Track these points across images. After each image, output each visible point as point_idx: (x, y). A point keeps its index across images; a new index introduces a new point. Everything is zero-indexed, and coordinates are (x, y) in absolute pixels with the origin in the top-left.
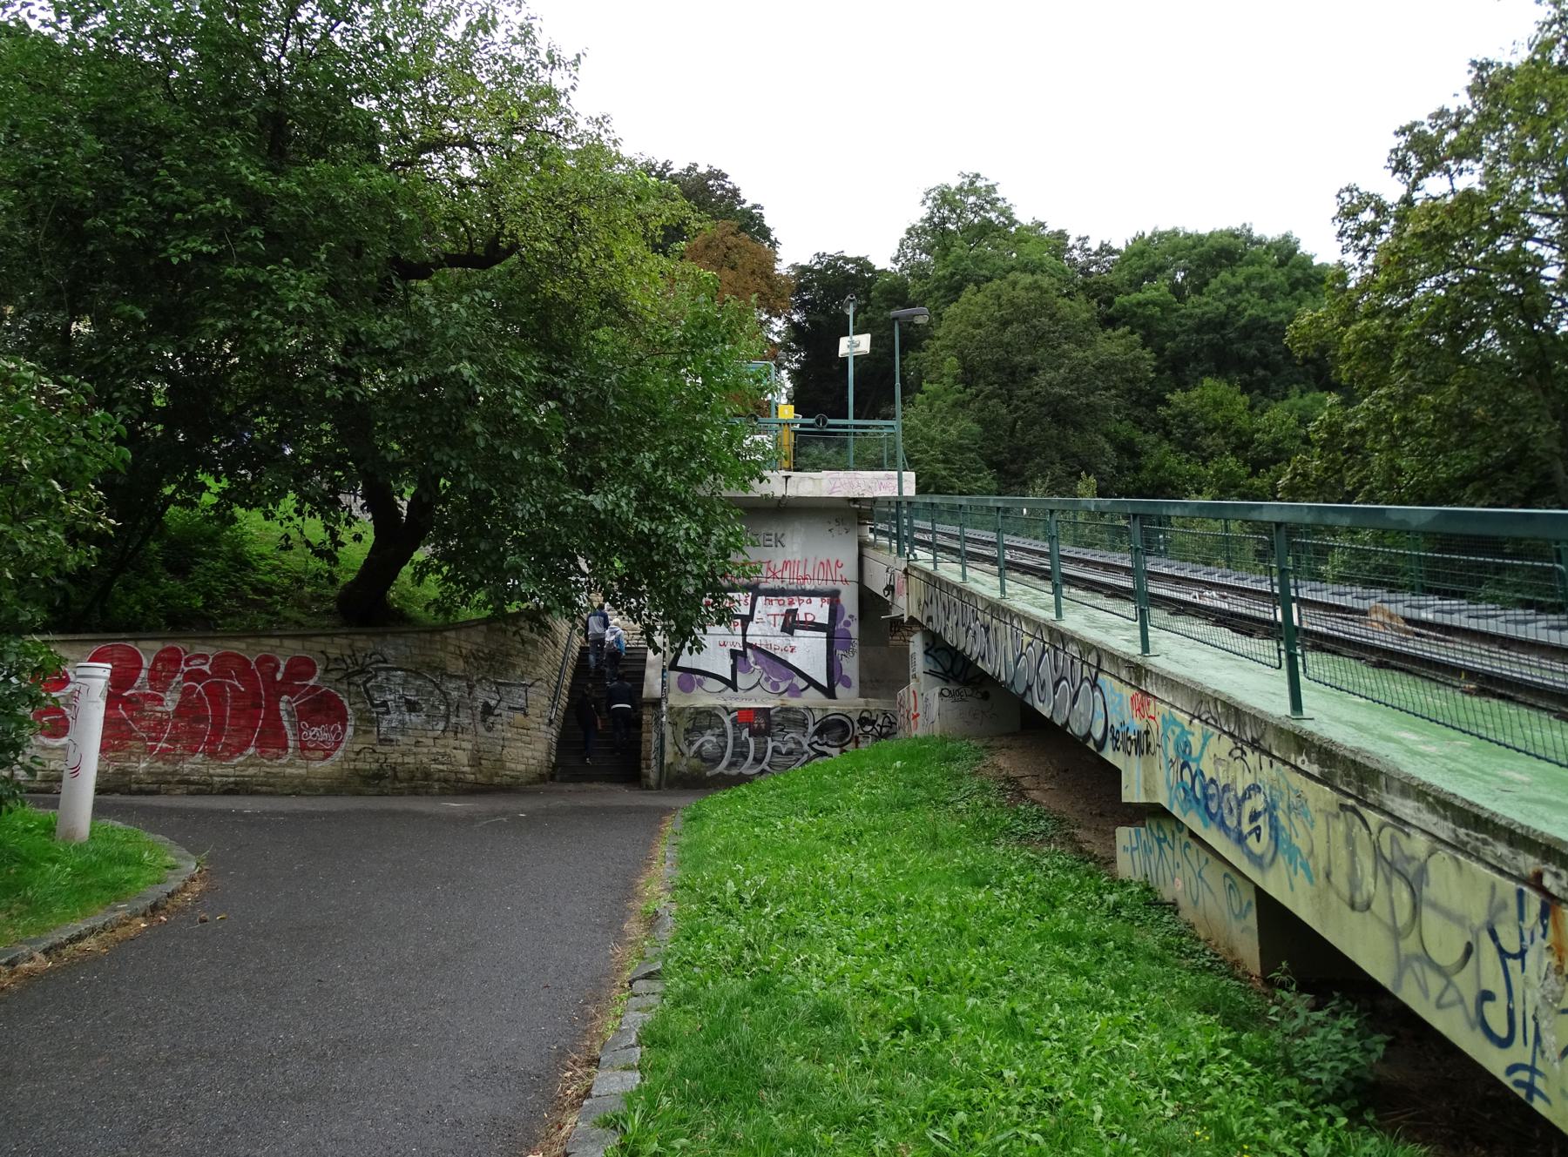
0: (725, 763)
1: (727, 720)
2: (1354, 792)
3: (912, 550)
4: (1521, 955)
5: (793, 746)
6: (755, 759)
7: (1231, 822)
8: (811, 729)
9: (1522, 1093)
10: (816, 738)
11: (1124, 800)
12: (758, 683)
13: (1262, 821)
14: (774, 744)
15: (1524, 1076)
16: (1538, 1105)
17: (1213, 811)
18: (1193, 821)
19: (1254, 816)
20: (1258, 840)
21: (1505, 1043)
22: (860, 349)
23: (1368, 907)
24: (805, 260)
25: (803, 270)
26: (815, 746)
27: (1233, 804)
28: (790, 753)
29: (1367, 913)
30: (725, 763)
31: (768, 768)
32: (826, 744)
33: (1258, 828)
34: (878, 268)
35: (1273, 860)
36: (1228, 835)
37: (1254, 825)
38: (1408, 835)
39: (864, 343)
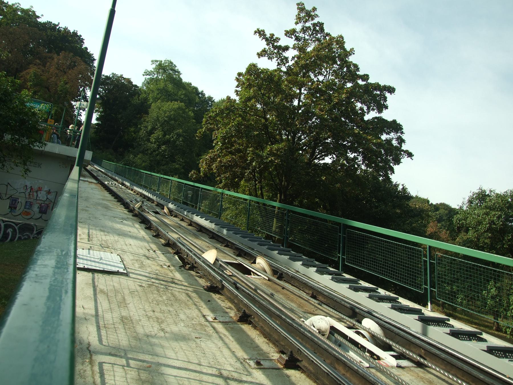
10: (36, 236)
12: (20, 214)
14: (20, 235)
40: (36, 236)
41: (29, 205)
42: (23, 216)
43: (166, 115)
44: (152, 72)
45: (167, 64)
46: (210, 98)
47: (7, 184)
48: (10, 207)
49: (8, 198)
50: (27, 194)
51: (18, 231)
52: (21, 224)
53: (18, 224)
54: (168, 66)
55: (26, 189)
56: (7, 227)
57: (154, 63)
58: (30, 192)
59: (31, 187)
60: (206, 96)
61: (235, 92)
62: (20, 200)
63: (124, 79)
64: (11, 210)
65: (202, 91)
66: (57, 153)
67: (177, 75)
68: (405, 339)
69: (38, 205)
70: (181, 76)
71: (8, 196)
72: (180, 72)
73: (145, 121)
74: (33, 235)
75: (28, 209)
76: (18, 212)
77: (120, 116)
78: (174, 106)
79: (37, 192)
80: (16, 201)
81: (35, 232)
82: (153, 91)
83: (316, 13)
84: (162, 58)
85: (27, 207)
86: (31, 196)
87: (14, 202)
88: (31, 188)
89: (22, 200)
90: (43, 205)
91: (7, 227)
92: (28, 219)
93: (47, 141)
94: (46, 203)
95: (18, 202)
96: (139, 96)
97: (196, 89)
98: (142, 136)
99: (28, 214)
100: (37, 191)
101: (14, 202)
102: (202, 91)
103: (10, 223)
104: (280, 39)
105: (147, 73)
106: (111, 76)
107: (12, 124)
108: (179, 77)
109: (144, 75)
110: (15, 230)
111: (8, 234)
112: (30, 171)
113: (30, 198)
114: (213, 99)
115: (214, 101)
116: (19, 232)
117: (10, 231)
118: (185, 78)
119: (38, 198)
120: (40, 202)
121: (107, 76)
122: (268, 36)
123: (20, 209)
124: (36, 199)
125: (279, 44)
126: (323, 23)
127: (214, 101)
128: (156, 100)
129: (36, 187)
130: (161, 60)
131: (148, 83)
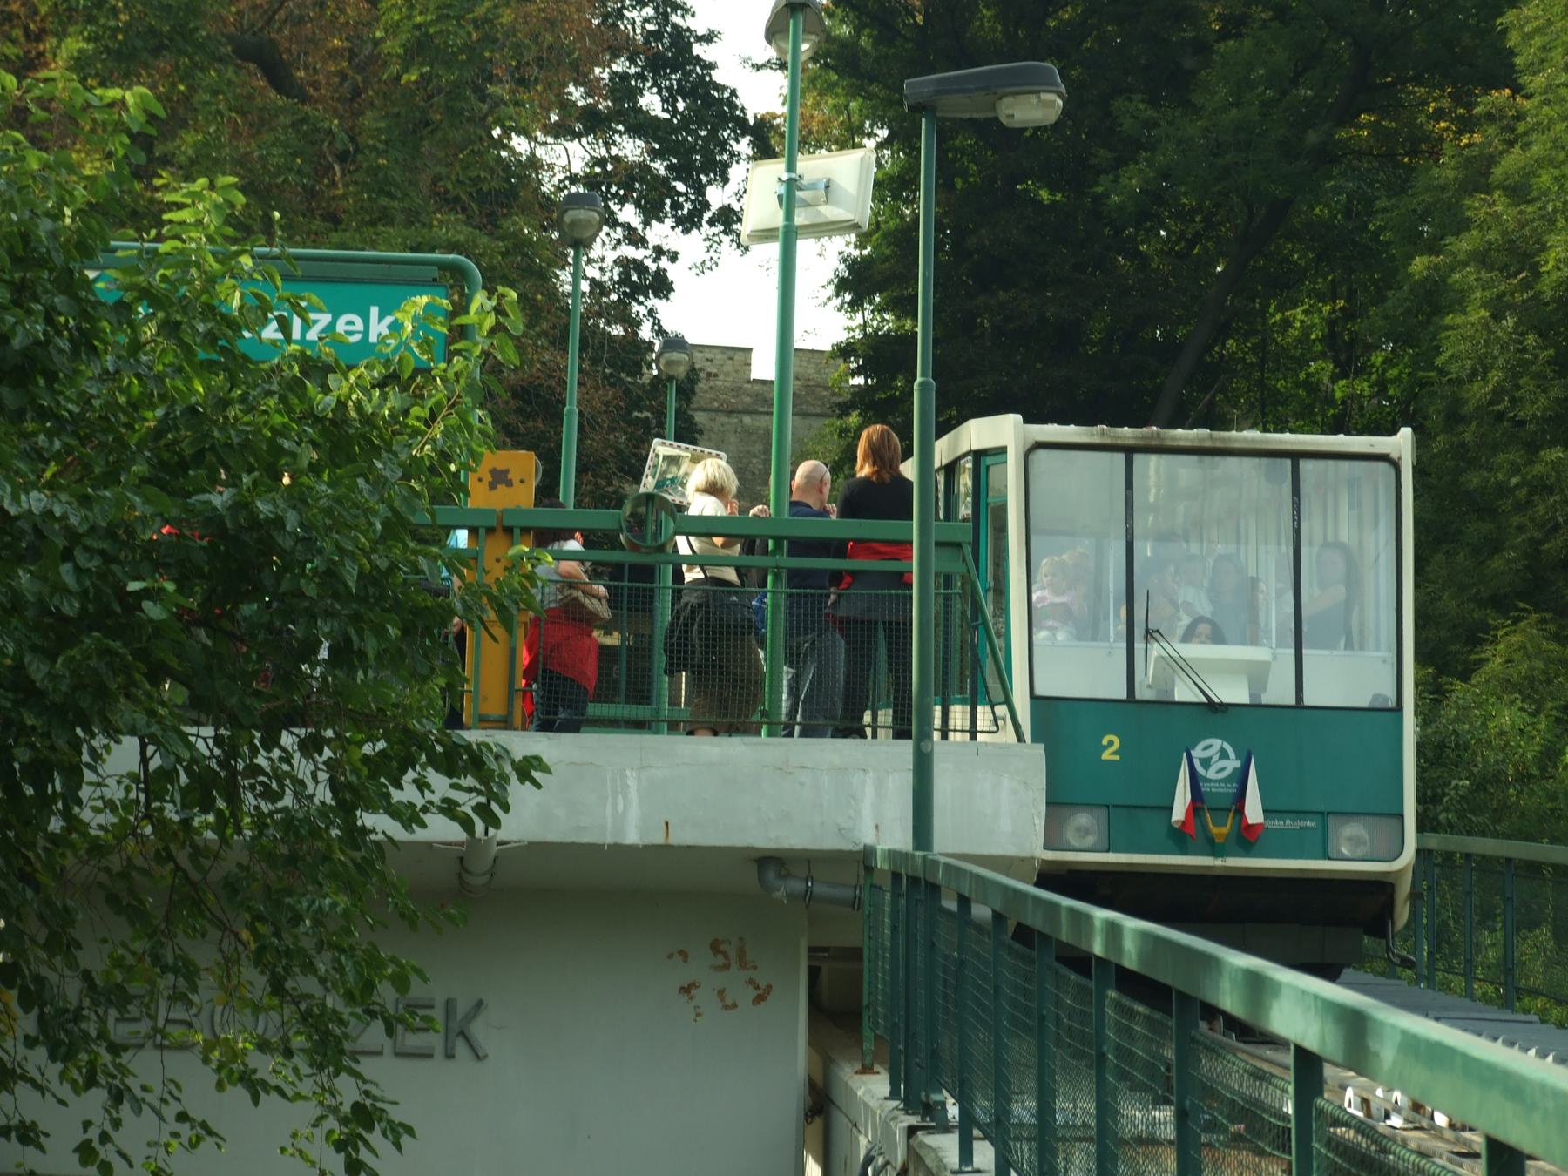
66: (632, 837)
68: (1280, 812)
73: (1478, 176)
77: (1133, 180)
93: (505, 723)
98: (1479, 391)
107: (153, 610)
112: (398, 1132)
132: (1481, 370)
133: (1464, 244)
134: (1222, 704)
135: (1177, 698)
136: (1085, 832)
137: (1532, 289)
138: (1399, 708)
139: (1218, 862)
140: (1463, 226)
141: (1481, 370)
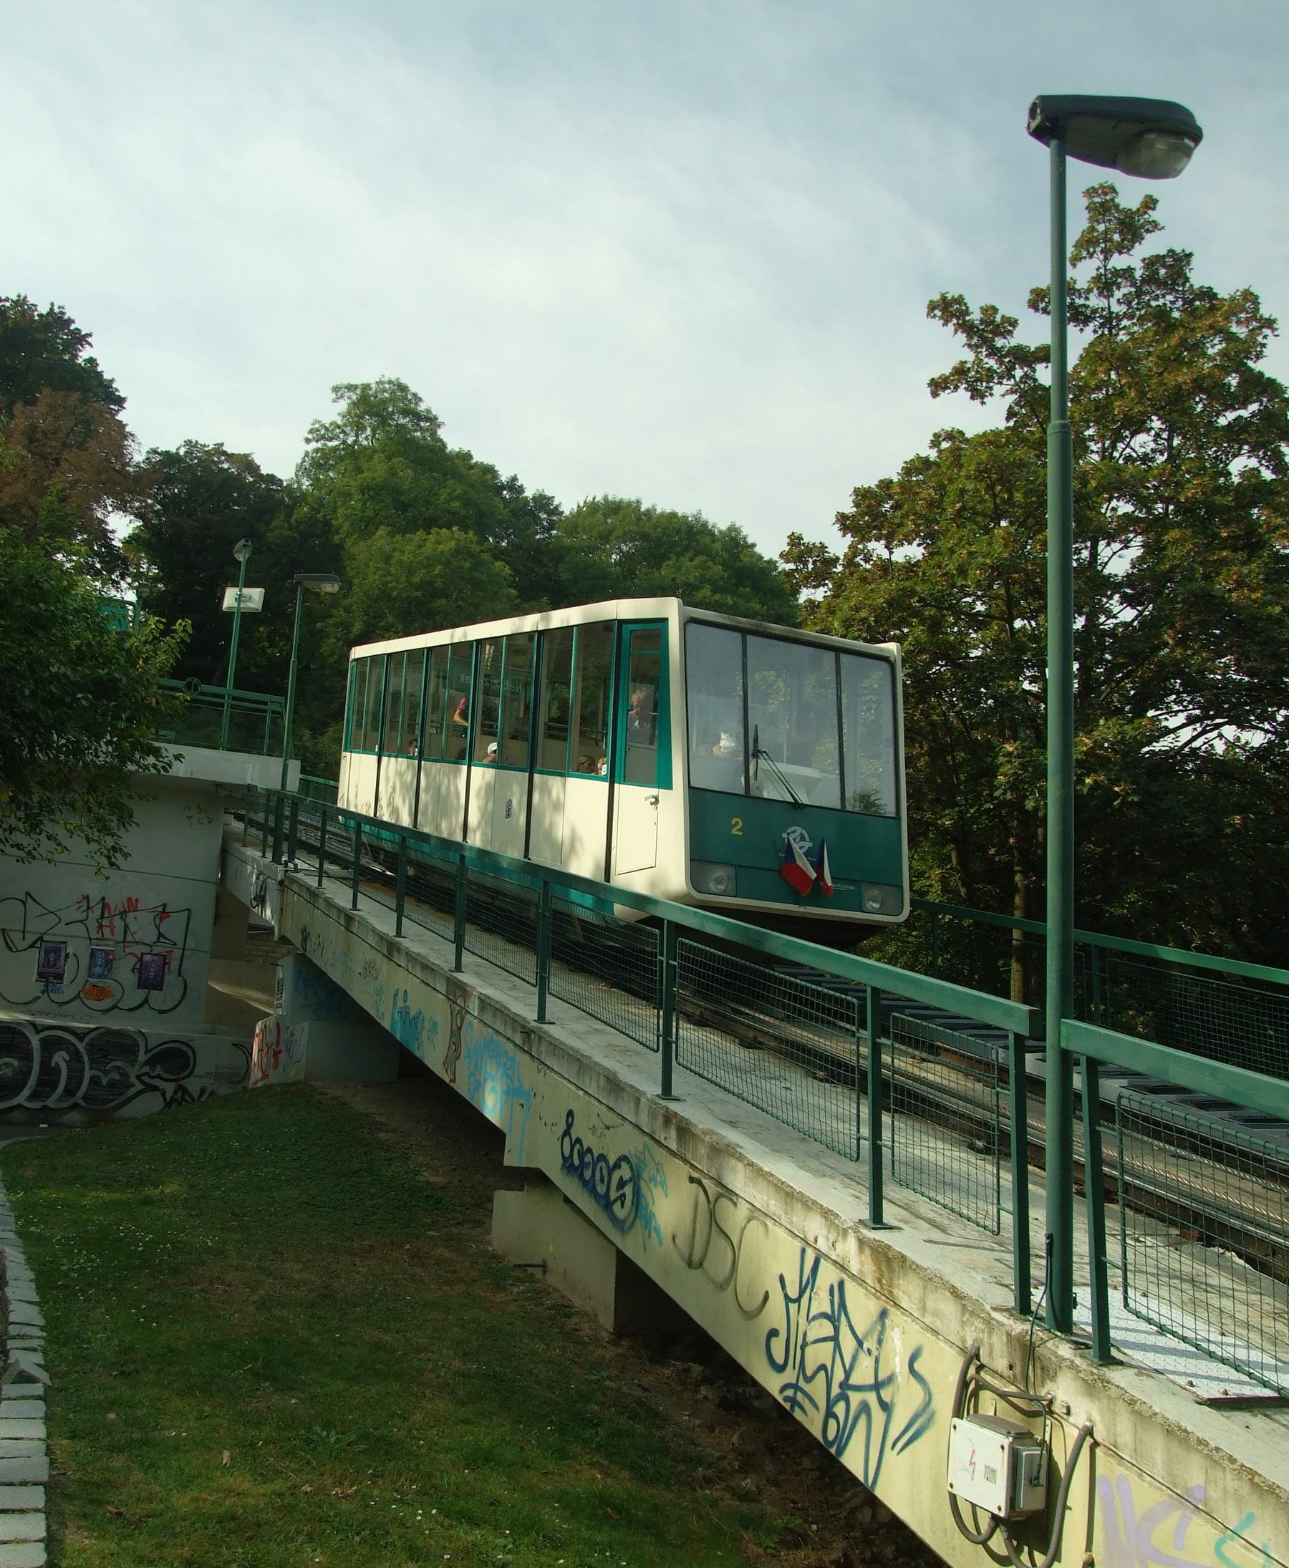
0: (26, 1092)
1: (35, 1040)
2: (1195, 744)
3: (291, 858)
4: (798, 1300)
5: (117, 1077)
6: (66, 1090)
7: (601, 1189)
8: (142, 1057)
9: (787, 1406)
10: (146, 1069)
11: (505, 1164)
12: (78, 996)
13: (628, 1190)
14: (94, 1072)
15: (790, 1392)
16: (798, 1414)
17: (587, 1178)
18: (569, 1187)
19: (622, 1184)
20: (622, 1207)
21: (780, 1369)
22: (250, 605)
23: (701, 1265)
24: (172, 444)
25: (169, 459)
26: (146, 1079)
27: (605, 1173)
28: (113, 1084)
29: (699, 1270)
30: (26, 1092)
31: (81, 1102)
32: (159, 1076)
33: (624, 1195)
34: (264, 471)
35: (633, 1224)
36: (598, 1202)
37: (621, 1192)
38: (735, 1204)
39: (255, 597)
40: (146, 1069)
41: (103, 962)
42: (86, 1001)
43: (416, 580)
44: (339, 427)
45: (386, 395)
46: (543, 502)
47: (23, 897)
48: (41, 975)
49: (32, 946)
50: (92, 925)
51: (86, 1059)
52: (98, 1031)
53: (85, 1035)
54: (393, 400)
55: (88, 908)
56: (50, 1046)
57: (342, 397)
58: (102, 917)
59: (103, 899)
60: (529, 493)
61: (837, 521)
62: (70, 950)
63: (230, 457)
64: (46, 986)
65: (514, 479)
67: (427, 430)
69: (133, 960)
70: (441, 433)
71: (31, 938)
72: (436, 418)
74: (137, 1067)
75: (100, 976)
76: (68, 988)
78: (441, 547)
79: (123, 914)
80: (57, 951)
81: (142, 1057)
82: (348, 496)
83: (1153, 215)
84: (370, 373)
85: (98, 970)
86: (107, 931)
87: (52, 956)
88: (105, 906)
89: (77, 948)
90: (148, 958)
91: (50, 1046)
92: (104, 1012)
94: (156, 950)
95: (67, 956)
96: (289, 515)
97: (489, 471)
98: (332, 660)
99: (101, 993)
100: (125, 912)
101: (52, 956)
102: (514, 479)
103: (60, 1033)
104: (1016, 321)
105: (321, 432)
106: (182, 452)
108: (434, 434)
109: (308, 441)
110: (76, 1056)
111: (57, 1070)
113: (103, 938)
114: (556, 503)
115: (556, 508)
116: (92, 1062)
117: (60, 1058)
118: (453, 440)
119: (129, 938)
120: (138, 950)
121: (167, 452)
122: (976, 316)
123: (74, 974)
124: (124, 942)
125: (1013, 341)
126: (1191, 255)
127: (556, 508)
128: (366, 527)
129: (116, 901)
130: (365, 381)
131: (317, 464)
132: (332, 654)
133: (331, 621)
134: (803, 804)
135: (766, 796)
136: (718, 881)
137: (959, 574)
138: (898, 817)
139: (802, 909)
140: (332, 616)
141: (332, 654)
